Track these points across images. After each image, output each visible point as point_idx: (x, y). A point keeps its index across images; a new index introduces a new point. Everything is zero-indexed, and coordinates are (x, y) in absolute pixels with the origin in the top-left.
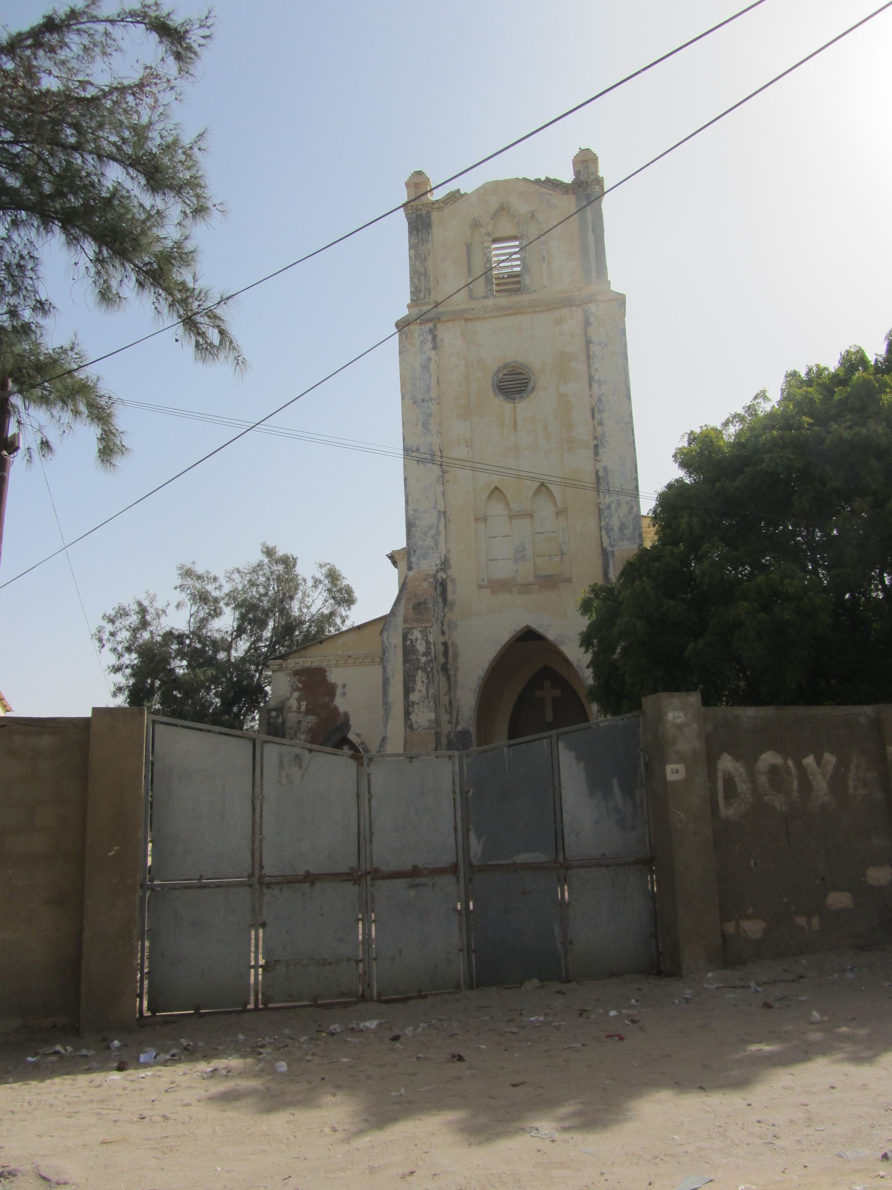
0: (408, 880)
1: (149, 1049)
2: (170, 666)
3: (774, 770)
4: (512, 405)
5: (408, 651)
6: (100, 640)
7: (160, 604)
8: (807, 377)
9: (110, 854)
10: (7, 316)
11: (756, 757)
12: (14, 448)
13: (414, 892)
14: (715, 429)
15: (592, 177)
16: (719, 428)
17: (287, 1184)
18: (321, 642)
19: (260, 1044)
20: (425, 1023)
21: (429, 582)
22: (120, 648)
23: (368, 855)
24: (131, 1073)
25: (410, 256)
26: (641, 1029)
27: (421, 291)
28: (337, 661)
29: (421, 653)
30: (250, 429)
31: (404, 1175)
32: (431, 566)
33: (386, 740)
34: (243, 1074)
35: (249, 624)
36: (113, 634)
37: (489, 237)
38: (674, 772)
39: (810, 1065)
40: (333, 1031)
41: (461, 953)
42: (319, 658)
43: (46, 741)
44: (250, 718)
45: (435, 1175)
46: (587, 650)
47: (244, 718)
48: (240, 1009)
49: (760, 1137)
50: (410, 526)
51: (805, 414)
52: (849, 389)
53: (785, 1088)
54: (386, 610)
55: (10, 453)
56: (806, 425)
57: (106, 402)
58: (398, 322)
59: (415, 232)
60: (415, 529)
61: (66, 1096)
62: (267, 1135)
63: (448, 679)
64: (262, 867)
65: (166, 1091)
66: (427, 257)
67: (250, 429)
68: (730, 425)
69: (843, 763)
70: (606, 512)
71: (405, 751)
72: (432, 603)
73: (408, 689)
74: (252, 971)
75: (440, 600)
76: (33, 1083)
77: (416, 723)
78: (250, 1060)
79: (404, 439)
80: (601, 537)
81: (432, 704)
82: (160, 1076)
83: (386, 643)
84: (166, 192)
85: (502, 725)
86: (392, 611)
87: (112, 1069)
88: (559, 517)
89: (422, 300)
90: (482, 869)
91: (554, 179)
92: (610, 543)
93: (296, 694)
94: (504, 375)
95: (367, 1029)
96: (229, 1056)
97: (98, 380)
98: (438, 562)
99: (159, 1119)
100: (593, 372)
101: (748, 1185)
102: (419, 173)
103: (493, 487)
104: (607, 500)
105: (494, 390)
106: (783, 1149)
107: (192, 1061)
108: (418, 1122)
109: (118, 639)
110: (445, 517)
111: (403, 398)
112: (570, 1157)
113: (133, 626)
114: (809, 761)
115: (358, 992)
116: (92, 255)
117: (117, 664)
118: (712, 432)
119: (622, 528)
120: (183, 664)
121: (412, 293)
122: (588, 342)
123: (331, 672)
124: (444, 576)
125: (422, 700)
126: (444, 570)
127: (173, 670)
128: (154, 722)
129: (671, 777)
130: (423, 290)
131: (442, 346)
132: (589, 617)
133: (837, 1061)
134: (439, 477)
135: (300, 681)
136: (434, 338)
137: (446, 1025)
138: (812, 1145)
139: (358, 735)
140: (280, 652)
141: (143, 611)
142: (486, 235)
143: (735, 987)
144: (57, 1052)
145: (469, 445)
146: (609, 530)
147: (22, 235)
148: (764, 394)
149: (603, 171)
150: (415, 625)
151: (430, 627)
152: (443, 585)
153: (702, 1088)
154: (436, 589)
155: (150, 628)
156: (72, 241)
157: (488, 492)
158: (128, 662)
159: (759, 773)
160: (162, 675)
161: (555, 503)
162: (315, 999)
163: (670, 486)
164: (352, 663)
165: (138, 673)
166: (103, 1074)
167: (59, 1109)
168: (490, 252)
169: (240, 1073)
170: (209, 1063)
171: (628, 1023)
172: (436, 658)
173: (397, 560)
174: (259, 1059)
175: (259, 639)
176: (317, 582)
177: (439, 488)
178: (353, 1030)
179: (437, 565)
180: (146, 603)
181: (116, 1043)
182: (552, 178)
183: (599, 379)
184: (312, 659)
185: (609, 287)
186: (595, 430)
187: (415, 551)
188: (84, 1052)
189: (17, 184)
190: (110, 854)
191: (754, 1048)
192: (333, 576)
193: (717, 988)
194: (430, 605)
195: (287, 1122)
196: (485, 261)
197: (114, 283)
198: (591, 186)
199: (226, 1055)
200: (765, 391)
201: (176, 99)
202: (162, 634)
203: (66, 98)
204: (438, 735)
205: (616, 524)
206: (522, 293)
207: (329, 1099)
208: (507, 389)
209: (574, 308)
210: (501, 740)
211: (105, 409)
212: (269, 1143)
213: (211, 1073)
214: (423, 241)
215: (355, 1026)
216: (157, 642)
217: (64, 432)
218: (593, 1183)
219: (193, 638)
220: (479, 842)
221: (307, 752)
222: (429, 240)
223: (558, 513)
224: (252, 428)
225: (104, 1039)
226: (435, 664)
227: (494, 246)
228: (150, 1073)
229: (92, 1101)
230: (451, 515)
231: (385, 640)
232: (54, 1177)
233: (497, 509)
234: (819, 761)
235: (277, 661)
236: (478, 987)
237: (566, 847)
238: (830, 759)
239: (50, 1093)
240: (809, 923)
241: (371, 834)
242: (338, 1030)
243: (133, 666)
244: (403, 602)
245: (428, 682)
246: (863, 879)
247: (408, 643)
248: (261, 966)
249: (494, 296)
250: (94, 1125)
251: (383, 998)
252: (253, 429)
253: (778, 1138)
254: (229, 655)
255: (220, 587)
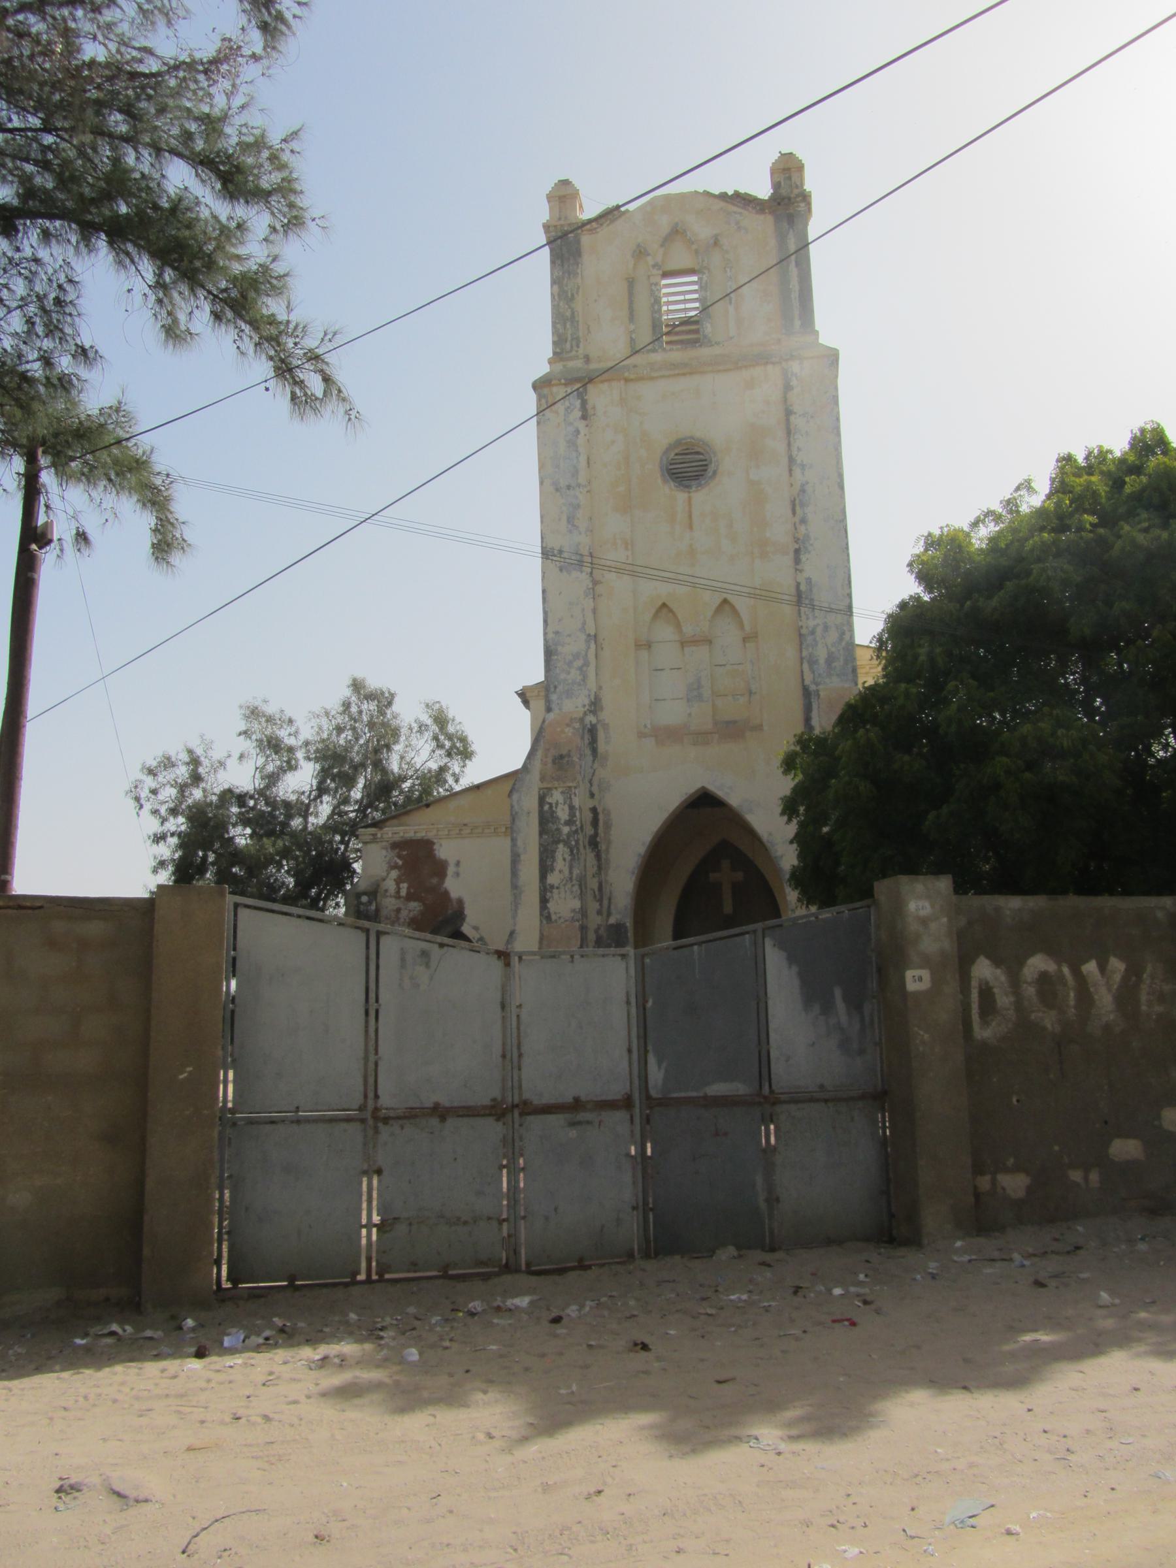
0: (567, 1116)
1: (234, 1330)
2: (228, 834)
3: (1044, 978)
4: (686, 495)
5: (546, 819)
6: (137, 799)
7: (217, 754)
8: (1086, 463)
9: (181, 1077)
10: (39, 363)
11: (1021, 963)
12: (45, 541)
13: (575, 1132)
14: (962, 530)
15: (796, 191)
16: (966, 529)
17: (436, 1504)
18: (428, 806)
19: (379, 1326)
20: (593, 1301)
21: (574, 728)
22: (163, 810)
23: (516, 1084)
24: (214, 1361)
25: (552, 294)
26: (878, 1312)
27: (566, 341)
28: (449, 831)
29: (562, 822)
30: (364, 521)
31: (589, 1494)
32: (577, 707)
33: (514, 935)
34: (360, 1363)
35: (333, 780)
36: (154, 792)
37: (658, 270)
38: (916, 980)
39: (1103, 1360)
40: (473, 1310)
41: (635, 1212)
42: (425, 827)
43: (95, 929)
44: (333, 903)
45: (630, 1495)
46: (790, 820)
47: (325, 904)
48: (348, 1280)
49: (1050, 1452)
50: (549, 653)
51: (1085, 511)
52: (1144, 479)
53: (1073, 1390)
54: (518, 764)
55: (41, 548)
56: (1088, 526)
57: (163, 482)
58: (535, 381)
59: (559, 262)
60: (556, 657)
61: (132, 1389)
62: (403, 1441)
63: (598, 857)
64: (377, 1097)
65: (264, 1385)
66: (576, 295)
67: (364, 521)
68: (981, 525)
69: (1134, 971)
70: (810, 639)
71: (540, 948)
72: (578, 756)
73: (545, 869)
74: (364, 1231)
75: (588, 752)
76: (88, 1372)
77: (555, 913)
78: (368, 1346)
79: (542, 538)
80: (802, 672)
81: (576, 888)
82: (253, 1365)
83: (516, 807)
84: (249, 199)
85: (665, 920)
86: (525, 766)
87: (189, 1356)
88: (747, 645)
89: (567, 352)
90: (664, 1102)
91: (746, 193)
92: (814, 679)
93: (394, 874)
94: (676, 454)
95: (517, 1307)
96: (340, 1341)
97: (152, 452)
98: (587, 702)
99: (259, 1420)
100: (794, 453)
101: (1041, 1512)
102: (565, 183)
103: (660, 603)
104: (811, 623)
105: (663, 475)
106: (1082, 1466)
107: (292, 1346)
108: (599, 1427)
109: (161, 797)
110: (596, 642)
111: (541, 483)
112: (804, 1473)
113: (179, 781)
114: (1090, 968)
115: (501, 1260)
116: (150, 277)
117: (159, 832)
118: (961, 534)
119: (830, 659)
120: (245, 832)
121: (554, 343)
122: (789, 413)
123: (441, 845)
124: (594, 720)
125: (564, 882)
126: (594, 712)
127: (232, 839)
128: (236, 906)
129: (911, 986)
130: (569, 338)
131: (594, 415)
132: (792, 776)
133: (1138, 1355)
134: (589, 589)
135: (399, 857)
136: (584, 403)
137: (619, 1304)
138: (1119, 1463)
139: (476, 928)
140: (374, 818)
141: (195, 762)
142: (654, 266)
143: (993, 1260)
144: (113, 1333)
145: (630, 547)
146: (813, 662)
147: (55, 253)
148: (1029, 484)
149: (810, 183)
150: (556, 784)
151: (575, 788)
152: (592, 731)
153: (965, 1388)
154: (582, 738)
155: (203, 785)
156: (123, 259)
157: (653, 611)
158: (173, 829)
159: (1026, 982)
160: (217, 845)
161: (741, 626)
162: (445, 1268)
163: (903, 605)
164: (470, 834)
165: (187, 843)
166: (178, 1362)
167: (126, 1406)
168: (659, 291)
169: (357, 1363)
170: (315, 1349)
171: (859, 1304)
172: (582, 827)
173: (529, 699)
174: (380, 1345)
175: (346, 801)
176: (422, 728)
177: (589, 604)
178: (498, 1309)
179: (584, 706)
180: (199, 751)
181: (190, 1322)
182: (742, 191)
183: (802, 461)
184: (415, 827)
185: (818, 339)
186: (796, 529)
187: (555, 687)
188: (149, 1333)
189: (50, 185)
190: (181, 1077)
191: (1028, 1338)
192: (441, 720)
193: (970, 1261)
194: (575, 759)
195: (427, 1425)
196: (653, 301)
197: (182, 317)
198: (793, 203)
199: (336, 1339)
200: (1030, 480)
201: (263, 74)
202: (218, 793)
203: (115, 70)
204: (583, 928)
205: (821, 654)
206: (701, 346)
207: (480, 1396)
208: (685, 472)
209: (770, 367)
210: (664, 941)
211: (160, 490)
212: (406, 1452)
213: (320, 1362)
214: (569, 274)
215: (501, 1304)
216: (211, 802)
217: (107, 520)
218: (838, 1507)
219: (258, 799)
220: (659, 1067)
221: (436, 947)
222: (578, 274)
223: (745, 640)
224: (367, 519)
225: (173, 1317)
226: (581, 836)
227: (664, 282)
228: (239, 1361)
229: (167, 1396)
230: (604, 639)
231: (515, 803)
232: (132, 1494)
233: (665, 632)
234: (1102, 968)
235: (369, 829)
236: (656, 1255)
237: (772, 1076)
238: (1117, 965)
239: (111, 1385)
240: (1086, 1179)
241: (520, 1055)
242: (479, 1309)
243: (181, 833)
244: (539, 754)
245: (571, 860)
246: (1156, 1123)
247: (546, 807)
248: (376, 1225)
249: (664, 350)
250: (174, 1427)
251: (533, 1268)
252: (362, 520)
253: (1073, 1453)
254: (306, 822)
255: (296, 734)
